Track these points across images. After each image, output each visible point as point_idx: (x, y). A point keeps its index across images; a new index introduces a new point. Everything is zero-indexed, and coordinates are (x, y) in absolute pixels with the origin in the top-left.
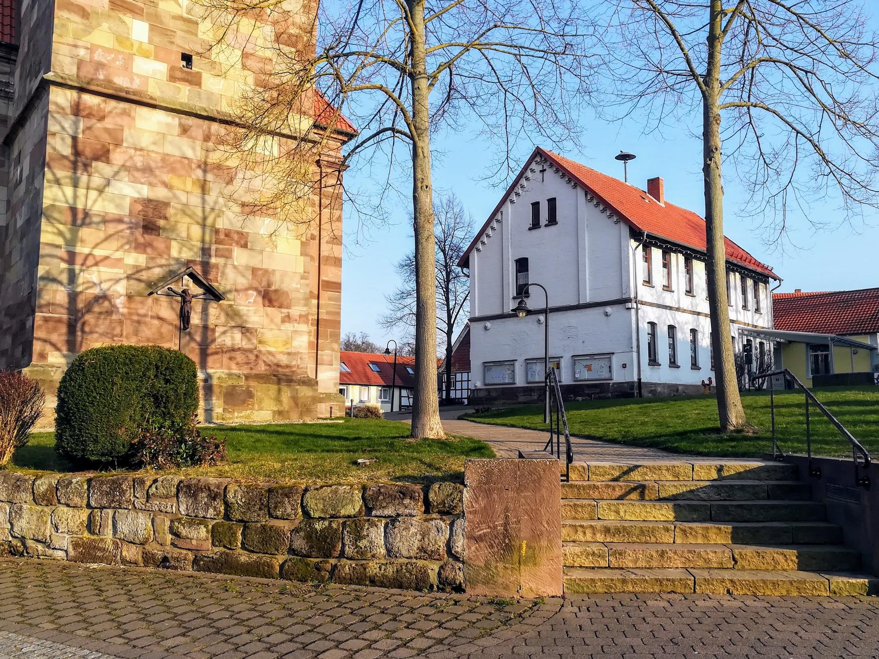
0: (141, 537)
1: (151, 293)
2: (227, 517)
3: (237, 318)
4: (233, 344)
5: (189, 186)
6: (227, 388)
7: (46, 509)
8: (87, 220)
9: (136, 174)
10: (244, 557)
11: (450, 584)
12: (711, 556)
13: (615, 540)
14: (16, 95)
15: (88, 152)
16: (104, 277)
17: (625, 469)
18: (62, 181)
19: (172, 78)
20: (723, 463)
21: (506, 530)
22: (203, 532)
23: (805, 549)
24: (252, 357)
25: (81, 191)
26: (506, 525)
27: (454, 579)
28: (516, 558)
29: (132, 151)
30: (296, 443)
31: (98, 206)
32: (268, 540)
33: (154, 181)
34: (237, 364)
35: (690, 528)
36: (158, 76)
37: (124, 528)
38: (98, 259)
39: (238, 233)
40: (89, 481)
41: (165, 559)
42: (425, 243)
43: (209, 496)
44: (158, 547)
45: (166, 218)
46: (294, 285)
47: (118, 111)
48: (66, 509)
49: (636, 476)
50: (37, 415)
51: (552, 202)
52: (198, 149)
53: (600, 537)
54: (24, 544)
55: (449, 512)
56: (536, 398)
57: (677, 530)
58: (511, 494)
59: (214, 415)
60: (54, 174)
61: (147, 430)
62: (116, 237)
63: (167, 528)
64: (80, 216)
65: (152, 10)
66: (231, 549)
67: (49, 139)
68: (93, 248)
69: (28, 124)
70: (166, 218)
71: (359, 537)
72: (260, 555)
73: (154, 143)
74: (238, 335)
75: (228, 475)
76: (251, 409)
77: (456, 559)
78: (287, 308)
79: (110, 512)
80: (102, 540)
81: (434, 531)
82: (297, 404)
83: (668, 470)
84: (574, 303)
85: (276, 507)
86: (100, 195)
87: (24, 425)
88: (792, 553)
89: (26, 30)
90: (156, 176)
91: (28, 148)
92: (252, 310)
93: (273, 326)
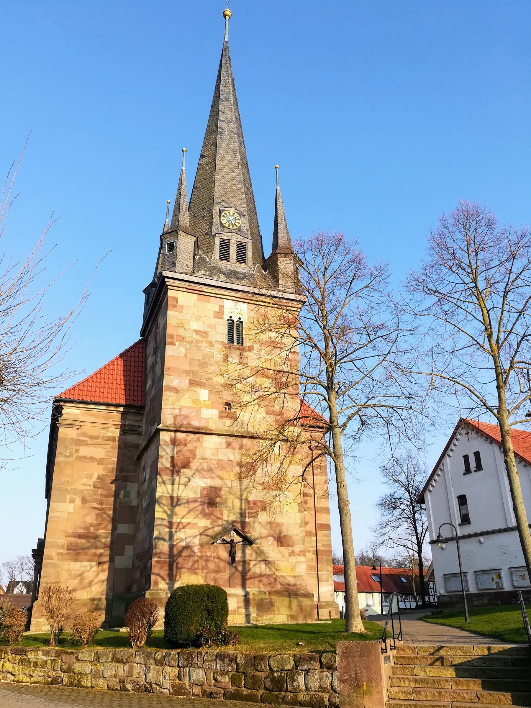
0: (201, 682)
1: (213, 543)
2: (237, 671)
3: (262, 555)
4: (261, 572)
5: (232, 477)
6: (258, 600)
7: (160, 668)
8: (179, 503)
9: (204, 473)
10: (245, 692)
11: (333, 705)
12: (465, 695)
13: (420, 686)
14: (143, 433)
15: (179, 464)
16: (188, 535)
17: (437, 648)
18: (166, 482)
19: (221, 417)
20: (490, 646)
21: (356, 677)
22: (227, 679)
23: (515, 693)
24: (272, 580)
25: (176, 486)
26: (356, 674)
27: (335, 703)
28: (362, 691)
29: (201, 461)
30: (286, 635)
31: (184, 493)
32: (254, 683)
33: (213, 475)
34: (264, 584)
35: (459, 680)
36: (214, 418)
37: (193, 677)
38: (184, 525)
39: (260, 501)
40: (178, 653)
41: (211, 693)
42: (344, 517)
43: (229, 660)
44: (208, 687)
45: (220, 497)
46: (295, 532)
47: (195, 439)
48: (169, 668)
49: (442, 653)
50: (156, 620)
51: (477, 455)
52: (237, 455)
53: (412, 684)
54: (151, 686)
55: (330, 668)
56: (486, 602)
57: (452, 681)
58: (357, 659)
59: (251, 618)
60: (162, 478)
61: (204, 627)
62: (193, 511)
63: (212, 677)
64: (175, 500)
65: (210, 383)
66: (239, 687)
67: (160, 459)
68: (182, 518)
69: (149, 449)
70: (220, 497)
71: (293, 681)
72: (252, 690)
73: (213, 454)
74: (263, 566)
75: (239, 650)
76: (273, 614)
77: (335, 692)
78: (292, 546)
79: (188, 669)
80: (184, 684)
81: (325, 677)
82: (302, 610)
83: (460, 649)
84: (504, 527)
85: (257, 665)
86: (185, 488)
87: (151, 626)
88: (508, 695)
89: (149, 399)
90: (214, 473)
91: (149, 463)
92: (270, 548)
93: (284, 559)
